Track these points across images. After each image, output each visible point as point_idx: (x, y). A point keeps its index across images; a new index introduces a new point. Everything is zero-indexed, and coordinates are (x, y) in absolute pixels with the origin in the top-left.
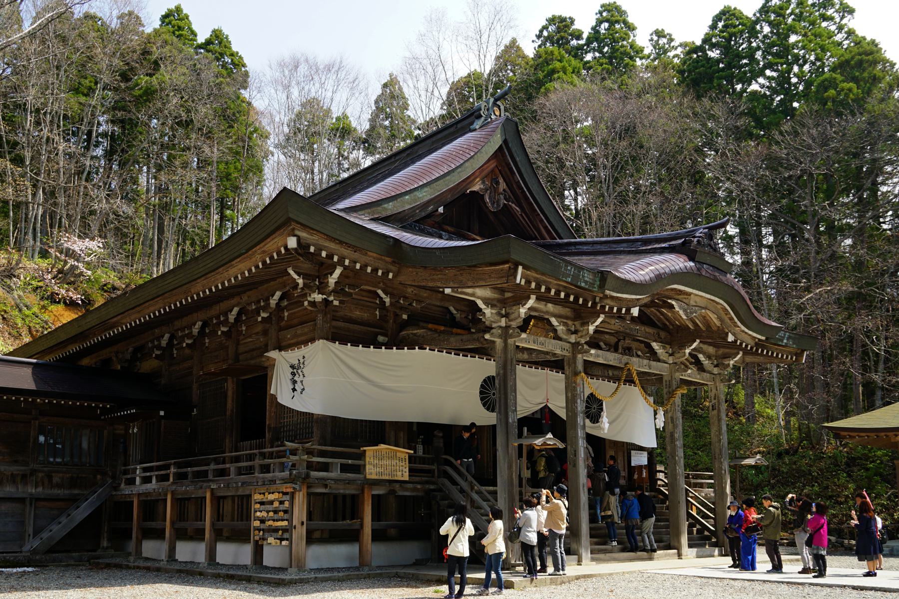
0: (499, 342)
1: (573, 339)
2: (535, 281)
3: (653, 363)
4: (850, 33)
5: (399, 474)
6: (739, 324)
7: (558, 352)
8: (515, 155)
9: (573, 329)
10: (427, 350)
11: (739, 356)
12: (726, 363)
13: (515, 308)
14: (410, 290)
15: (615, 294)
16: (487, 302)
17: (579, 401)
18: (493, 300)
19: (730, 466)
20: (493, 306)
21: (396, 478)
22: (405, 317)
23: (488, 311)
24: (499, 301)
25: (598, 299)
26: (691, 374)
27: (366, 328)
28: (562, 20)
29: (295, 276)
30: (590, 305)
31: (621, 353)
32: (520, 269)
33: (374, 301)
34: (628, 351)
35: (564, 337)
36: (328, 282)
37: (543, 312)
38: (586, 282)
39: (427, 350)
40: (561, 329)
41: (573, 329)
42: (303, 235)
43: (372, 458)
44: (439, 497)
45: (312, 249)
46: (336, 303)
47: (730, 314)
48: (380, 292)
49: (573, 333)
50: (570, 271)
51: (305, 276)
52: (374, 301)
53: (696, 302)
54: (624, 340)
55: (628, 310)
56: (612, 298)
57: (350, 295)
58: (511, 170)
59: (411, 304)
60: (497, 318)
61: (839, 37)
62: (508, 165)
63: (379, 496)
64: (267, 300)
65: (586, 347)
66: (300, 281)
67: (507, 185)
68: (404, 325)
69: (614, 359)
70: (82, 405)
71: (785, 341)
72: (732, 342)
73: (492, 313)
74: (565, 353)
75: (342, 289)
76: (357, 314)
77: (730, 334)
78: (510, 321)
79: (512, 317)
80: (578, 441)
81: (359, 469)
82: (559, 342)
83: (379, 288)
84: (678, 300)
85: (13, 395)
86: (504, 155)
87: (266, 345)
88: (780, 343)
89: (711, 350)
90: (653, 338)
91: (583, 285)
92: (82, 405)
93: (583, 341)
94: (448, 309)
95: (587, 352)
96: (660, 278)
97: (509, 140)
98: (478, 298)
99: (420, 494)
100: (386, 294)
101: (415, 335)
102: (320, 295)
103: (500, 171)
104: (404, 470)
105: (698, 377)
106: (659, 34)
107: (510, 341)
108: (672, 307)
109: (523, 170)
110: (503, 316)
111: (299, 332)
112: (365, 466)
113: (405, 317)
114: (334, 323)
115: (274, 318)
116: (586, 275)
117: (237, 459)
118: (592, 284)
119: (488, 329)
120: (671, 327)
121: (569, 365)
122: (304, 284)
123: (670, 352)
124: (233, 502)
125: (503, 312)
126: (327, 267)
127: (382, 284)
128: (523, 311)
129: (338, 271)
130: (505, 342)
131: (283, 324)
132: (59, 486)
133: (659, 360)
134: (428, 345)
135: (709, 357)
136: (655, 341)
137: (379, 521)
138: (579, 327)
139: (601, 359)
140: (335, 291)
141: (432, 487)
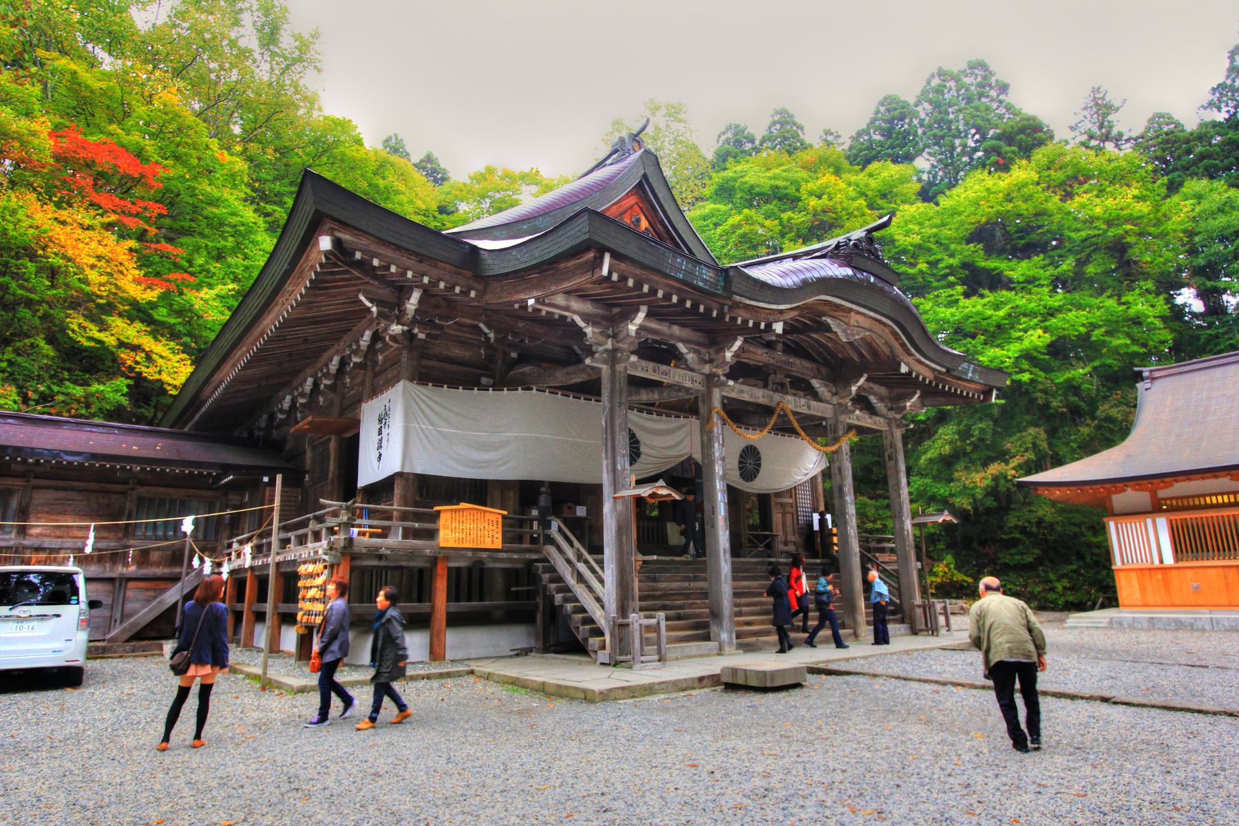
0: (605, 368)
1: (707, 369)
2: (633, 278)
3: (813, 403)
4: (1008, 108)
5: (488, 540)
6: (913, 351)
7: (688, 384)
8: (657, 191)
9: (707, 358)
10: (534, 391)
11: (917, 396)
12: (902, 405)
13: (622, 325)
14: (521, 324)
15: (748, 302)
16: (587, 318)
17: (716, 445)
18: (595, 316)
19: (913, 525)
20: (595, 324)
21: (483, 546)
22: (514, 355)
23: (589, 330)
24: (604, 318)
25: (726, 309)
26: (859, 417)
27: (466, 369)
28: (737, 126)
29: (368, 304)
30: (715, 314)
31: (772, 390)
32: (607, 259)
33: (478, 338)
34: (780, 388)
35: (696, 367)
36: (406, 309)
37: (666, 335)
38: (704, 281)
39: (534, 391)
40: (690, 357)
41: (707, 358)
42: (346, 237)
43: (449, 521)
44: (541, 570)
45: (358, 255)
46: (422, 336)
47: (901, 339)
48: (482, 325)
49: (706, 362)
50: (681, 264)
51: (379, 303)
52: (478, 338)
53: (857, 322)
54: (775, 373)
55: (769, 326)
56: (747, 307)
57: (441, 327)
58: (653, 207)
59: (522, 341)
60: (601, 339)
61: (1002, 111)
62: (650, 202)
63: (458, 569)
64: (357, 342)
65: (723, 378)
66: (374, 309)
67: (650, 223)
68: (513, 364)
69: (763, 397)
70: (163, 471)
71: (970, 375)
72: (906, 374)
73: (594, 333)
74: (697, 386)
75: (431, 321)
76: (456, 352)
77: (903, 364)
78: (618, 342)
79: (621, 336)
80: (716, 494)
81: (432, 534)
82: (689, 373)
83: (481, 321)
84: (834, 317)
85: (119, 462)
86: (645, 192)
87: (361, 394)
88: (964, 377)
89: (883, 390)
90: (812, 374)
91: (701, 284)
92: (163, 471)
93: (720, 372)
94: (571, 348)
95: (724, 384)
96: (807, 286)
97: (649, 175)
98: (575, 312)
99: (518, 566)
100: (489, 328)
101: (522, 374)
102: (400, 327)
103: (641, 208)
104: (496, 535)
105: (869, 421)
106: (828, 133)
107: (620, 367)
108: (828, 328)
109: (666, 207)
110: (609, 337)
111: (389, 376)
112: (438, 530)
113: (514, 355)
114: (425, 362)
115: (369, 364)
116: (704, 271)
117: (359, 526)
118: (715, 285)
119: (590, 352)
120: (833, 362)
121: (704, 402)
122: (379, 313)
123: (834, 390)
124: (402, 573)
125: (610, 332)
126: (403, 291)
127: (483, 317)
128: (632, 328)
129: (416, 296)
130: (613, 368)
131: (378, 369)
132: (158, 564)
133: (821, 401)
134: (534, 384)
135: (881, 399)
136: (815, 377)
137: (457, 600)
138: (713, 356)
139: (745, 395)
140: (414, 321)
141: (534, 557)
